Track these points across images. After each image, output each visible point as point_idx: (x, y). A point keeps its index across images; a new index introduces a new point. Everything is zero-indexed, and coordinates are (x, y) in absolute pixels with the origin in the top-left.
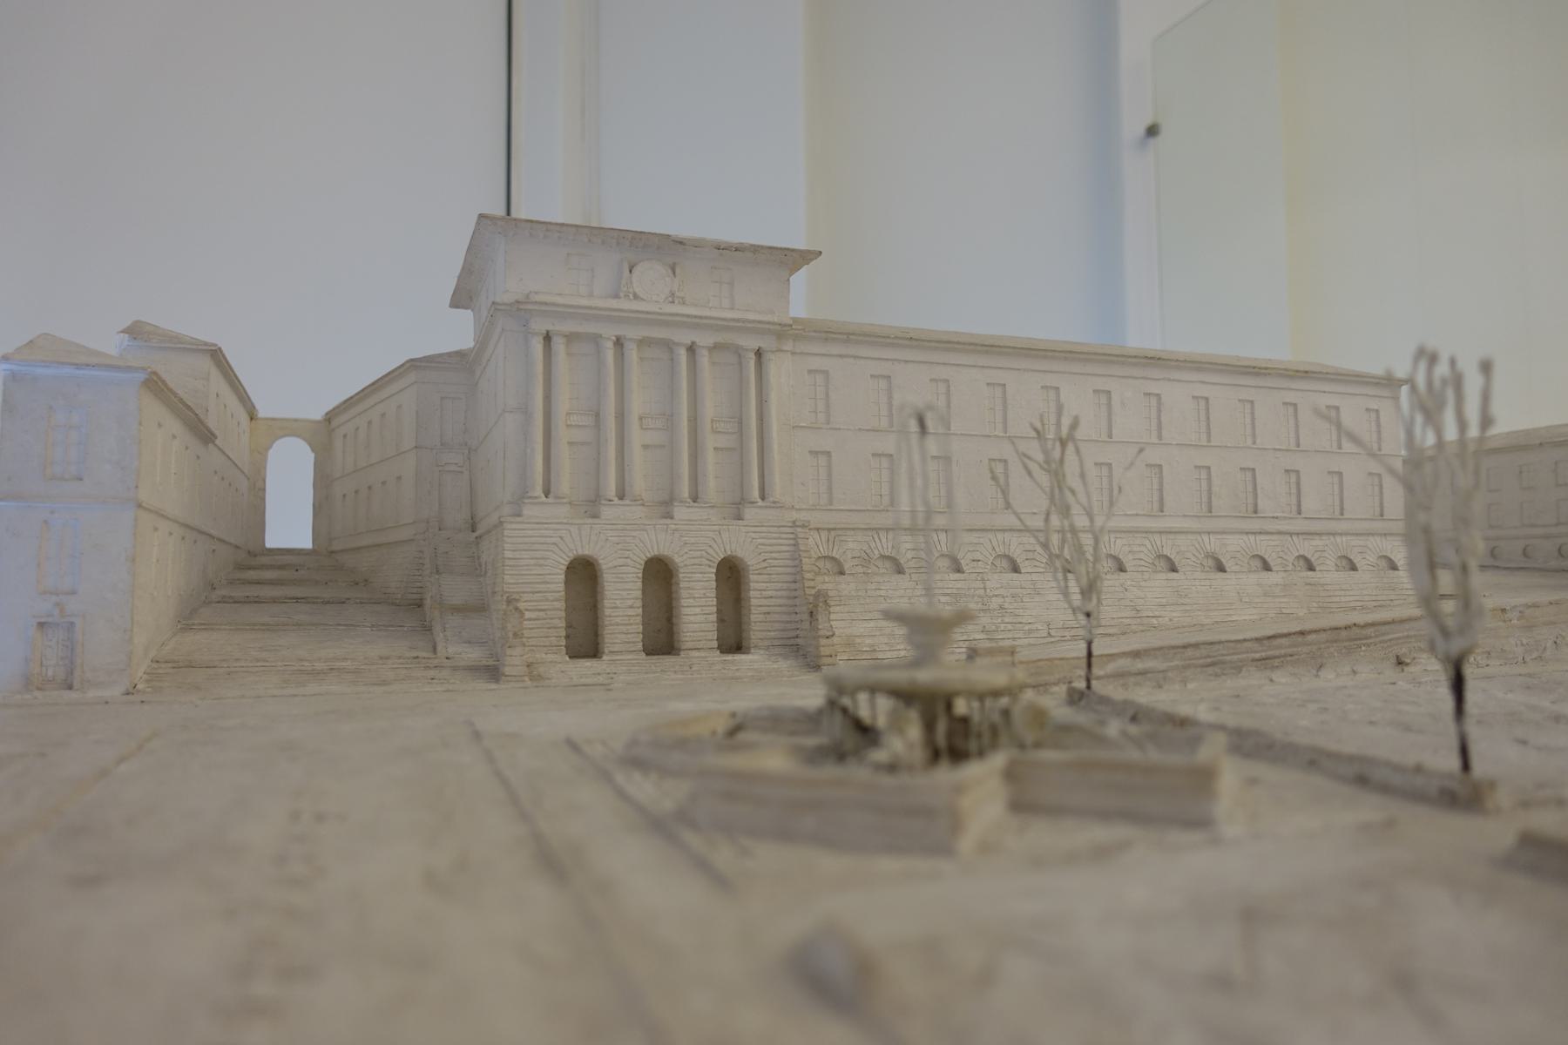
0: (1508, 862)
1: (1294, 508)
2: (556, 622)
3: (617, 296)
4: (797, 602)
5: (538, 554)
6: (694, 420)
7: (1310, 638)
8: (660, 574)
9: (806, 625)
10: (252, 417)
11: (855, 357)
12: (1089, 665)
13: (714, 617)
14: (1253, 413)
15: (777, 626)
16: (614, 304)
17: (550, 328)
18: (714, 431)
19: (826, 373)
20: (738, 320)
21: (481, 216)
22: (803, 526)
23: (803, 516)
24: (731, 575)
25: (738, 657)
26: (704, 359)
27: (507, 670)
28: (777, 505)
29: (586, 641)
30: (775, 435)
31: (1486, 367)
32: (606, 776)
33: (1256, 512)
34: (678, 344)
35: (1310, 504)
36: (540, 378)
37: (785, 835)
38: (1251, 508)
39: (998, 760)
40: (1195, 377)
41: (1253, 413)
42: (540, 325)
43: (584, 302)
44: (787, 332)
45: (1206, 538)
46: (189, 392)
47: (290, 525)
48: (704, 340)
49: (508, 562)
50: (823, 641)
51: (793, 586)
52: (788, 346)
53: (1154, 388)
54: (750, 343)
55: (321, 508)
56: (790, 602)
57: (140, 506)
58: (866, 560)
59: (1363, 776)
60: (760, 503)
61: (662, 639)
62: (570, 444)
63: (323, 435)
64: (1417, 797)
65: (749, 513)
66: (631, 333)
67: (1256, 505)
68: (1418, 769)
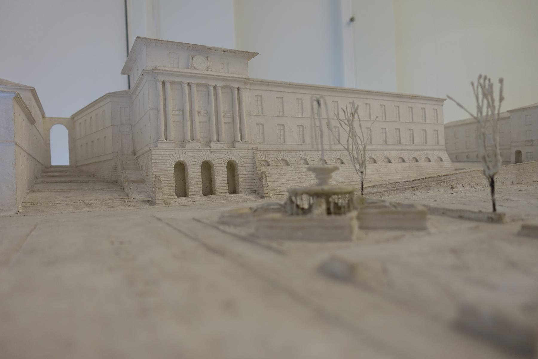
0: (519, 234)
1: (412, 142)
2: (172, 184)
3: (188, 68)
4: (255, 175)
5: (164, 161)
6: (217, 113)
7: (426, 180)
8: (207, 167)
9: (258, 183)
10: (43, 117)
11: (271, 91)
12: (362, 189)
13: (226, 182)
14: (399, 110)
15: (248, 184)
16: (187, 71)
17: (165, 79)
18: (224, 117)
19: (261, 96)
20: (231, 77)
21: (138, 37)
22: (256, 150)
23: (255, 146)
24: (231, 167)
25: (235, 195)
26: (220, 91)
27: (157, 201)
28: (246, 142)
29: (182, 191)
30: (245, 118)
31: (501, 81)
32: (217, 228)
33: (400, 143)
34: (211, 86)
35: (416, 140)
36: (162, 98)
37: (291, 238)
38: (399, 142)
39: (354, 214)
40: (381, 98)
41: (399, 110)
42: (161, 78)
43: (176, 70)
44: (247, 81)
45: (385, 152)
46: (26, 102)
47: (60, 157)
48: (220, 84)
49: (153, 164)
50: (265, 188)
51: (253, 170)
52: (248, 87)
53: (368, 102)
54: (235, 85)
55: (72, 150)
56: (252, 176)
57: (16, 144)
58: (277, 161)
59: (461, 216)
60: (241, 142)
61: (209, 190)
62: (174, 121)
63: (71, 123)
64: (478, 220)
65: (237, 145)
66: (194, 81)
67: (400, 141)
68: (480, 212)
